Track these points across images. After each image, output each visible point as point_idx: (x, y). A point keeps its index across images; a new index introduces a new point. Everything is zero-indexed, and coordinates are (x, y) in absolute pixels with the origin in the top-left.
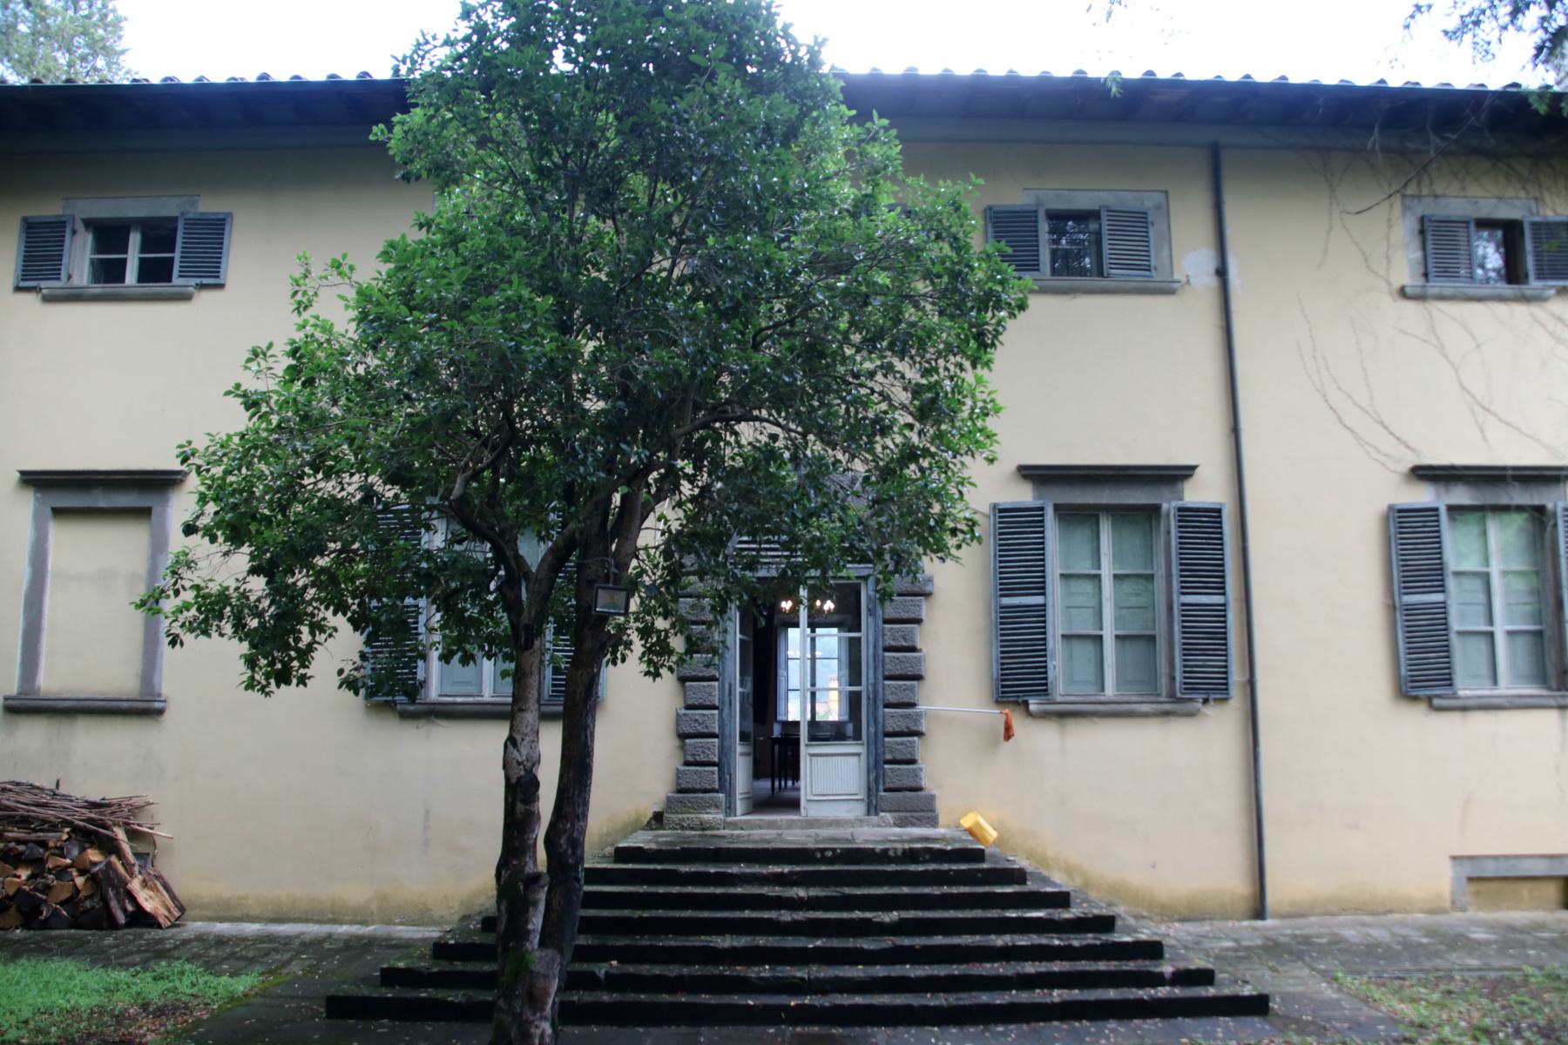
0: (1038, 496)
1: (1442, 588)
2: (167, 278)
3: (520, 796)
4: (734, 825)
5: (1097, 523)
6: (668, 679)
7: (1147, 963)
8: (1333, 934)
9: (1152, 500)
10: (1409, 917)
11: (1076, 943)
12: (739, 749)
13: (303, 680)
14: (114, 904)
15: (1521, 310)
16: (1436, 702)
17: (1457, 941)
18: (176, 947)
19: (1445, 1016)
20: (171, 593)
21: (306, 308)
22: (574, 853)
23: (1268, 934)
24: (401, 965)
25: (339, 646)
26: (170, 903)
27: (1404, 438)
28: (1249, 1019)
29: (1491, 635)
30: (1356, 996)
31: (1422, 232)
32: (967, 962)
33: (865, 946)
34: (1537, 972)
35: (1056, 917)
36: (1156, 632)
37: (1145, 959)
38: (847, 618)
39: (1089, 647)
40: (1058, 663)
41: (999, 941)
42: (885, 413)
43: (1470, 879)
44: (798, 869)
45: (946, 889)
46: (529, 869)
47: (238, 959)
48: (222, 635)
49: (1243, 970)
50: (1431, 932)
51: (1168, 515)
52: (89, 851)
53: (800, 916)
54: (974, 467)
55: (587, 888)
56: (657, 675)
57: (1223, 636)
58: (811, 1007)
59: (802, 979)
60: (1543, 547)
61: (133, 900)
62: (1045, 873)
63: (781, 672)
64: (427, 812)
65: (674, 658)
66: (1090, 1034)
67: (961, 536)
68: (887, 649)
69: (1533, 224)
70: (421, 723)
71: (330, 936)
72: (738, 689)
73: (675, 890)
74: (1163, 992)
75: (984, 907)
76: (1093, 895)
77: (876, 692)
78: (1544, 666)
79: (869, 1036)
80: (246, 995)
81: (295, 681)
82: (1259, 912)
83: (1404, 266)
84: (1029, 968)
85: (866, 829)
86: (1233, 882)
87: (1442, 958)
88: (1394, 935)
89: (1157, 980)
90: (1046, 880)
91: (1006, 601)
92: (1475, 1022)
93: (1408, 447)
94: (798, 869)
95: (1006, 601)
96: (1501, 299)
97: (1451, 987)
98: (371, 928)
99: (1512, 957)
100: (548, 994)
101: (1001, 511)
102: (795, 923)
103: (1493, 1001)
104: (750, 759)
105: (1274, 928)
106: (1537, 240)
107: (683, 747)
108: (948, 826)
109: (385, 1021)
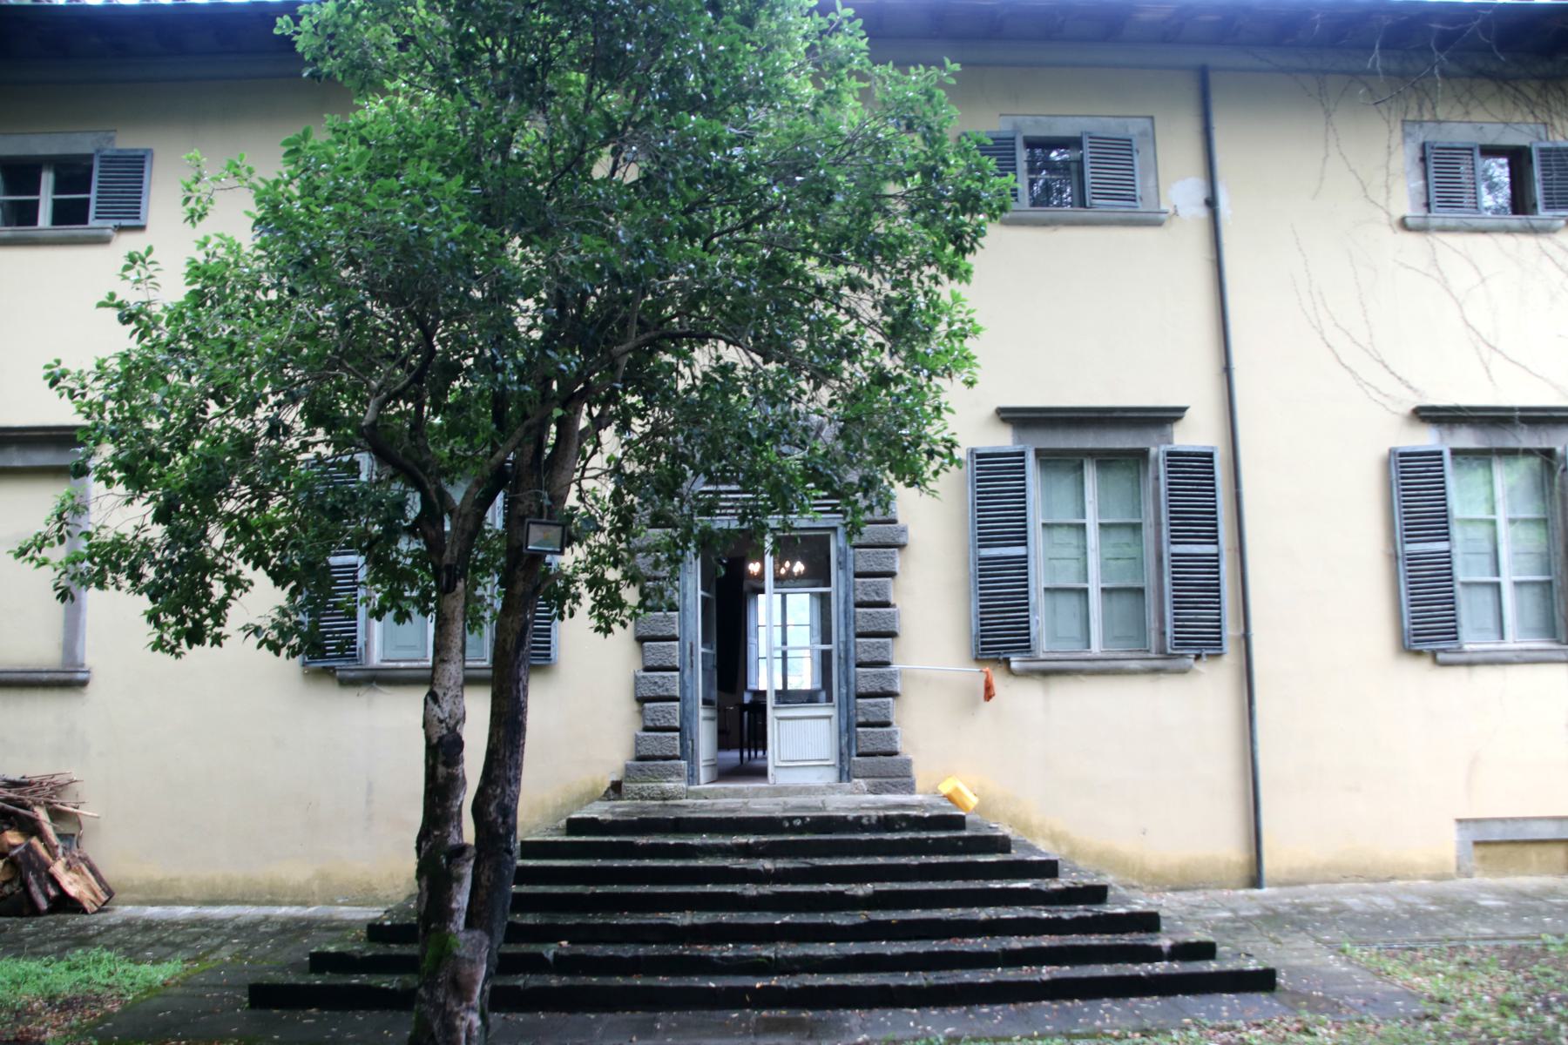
0: (1019, 440)
1: (1446, 537)
2: (84, 220)
3: (441, 758)
4: (698, 795)
5: (1081, 467)
6: (622, 637)
7: (1143, 936)
8: (1333, 903)
9: (1139, 445)
10: (1412, 883)
11: (1065, 916)
12: (702, 713)
13: (218, 640)
14: (35, 889)
15: (1528, 241)
16: (1440, 656)
17: (1466, 908)
18: (100, 934)
19: (1465, 991)
20: (55, 540)
21: (200, 217)
22: (504, 822)
23: (1267, 903)
24: (332, 949)
25: (262, 599)
26: (97, 887)
27: (1405, 377)
28: (1255, 996)
29: (1498, 586)
30: (1367, 969)
31: (1423, 159)
32: (949, 937)
33: (837, 922)
34: (1556, 941)
35: (1043, 888)
36: (1145, 584)
37: (1140, 931)
38: (819, 573)
39: (1074, 600)
40: (1041, 618)
41: (983, 914)
42: (854, 334)
43: (1476, 843)
44: (764, 839)
45: (924, 859)
46: (453, 840)
47: (165, 945)
48: (118, 588)
49: (1246, 942)
50: (1438, 899)
51: (1157, 460)
52: (8, 833)
53: (767, 889)
54: (950, 390)
55: (520, 862)
56: (608, 630)
57: (1216, 588)
58: (778, 989)
59: (769, 958)
60: (1551, 493)
61: (56, 883)
62: (1029, 841)
63: (751, 639)
64: (370, 789)
65: (627, 612)
66: (1083, 1015)
67: (938, 459)
68: (859, 605)
69: (1542, 150)
70: (362, 690)
71: (267, 918)
72: (701, 650)
73: (631, 863)
74: (1161, 967)
75: (965, 878)
76: (1080, 864)
77: (847, 651)
78: (1553, 619)
79: (841, 1020)
80: (165, 985)
81: (209, 641)
82: (1256, 881)
83: (1404, 196)
84: (1016, 943)
85: (838, 797)
86: (1229, 850)
87: (1453, 926)
88: (1399, 903)
89: (1154, 954)
90: (1031, 849)
91: (986, 552)
92: (1499, 995)
93: (1410, 387)
94: (764, 839)
95: (986, 552)
96: (1508, 230)
97: (1467, 958)
98: (312, 909)
99: (1526, 924)
100: (475, 982)
101: (979, 456)
102: (761, 897)
103: (1515, 973)
104: (713, 725)
105: (1273, 897)
106: (1545, 166)
107: (642, 712)
108: (925, 793)
109: (313, 1010)
